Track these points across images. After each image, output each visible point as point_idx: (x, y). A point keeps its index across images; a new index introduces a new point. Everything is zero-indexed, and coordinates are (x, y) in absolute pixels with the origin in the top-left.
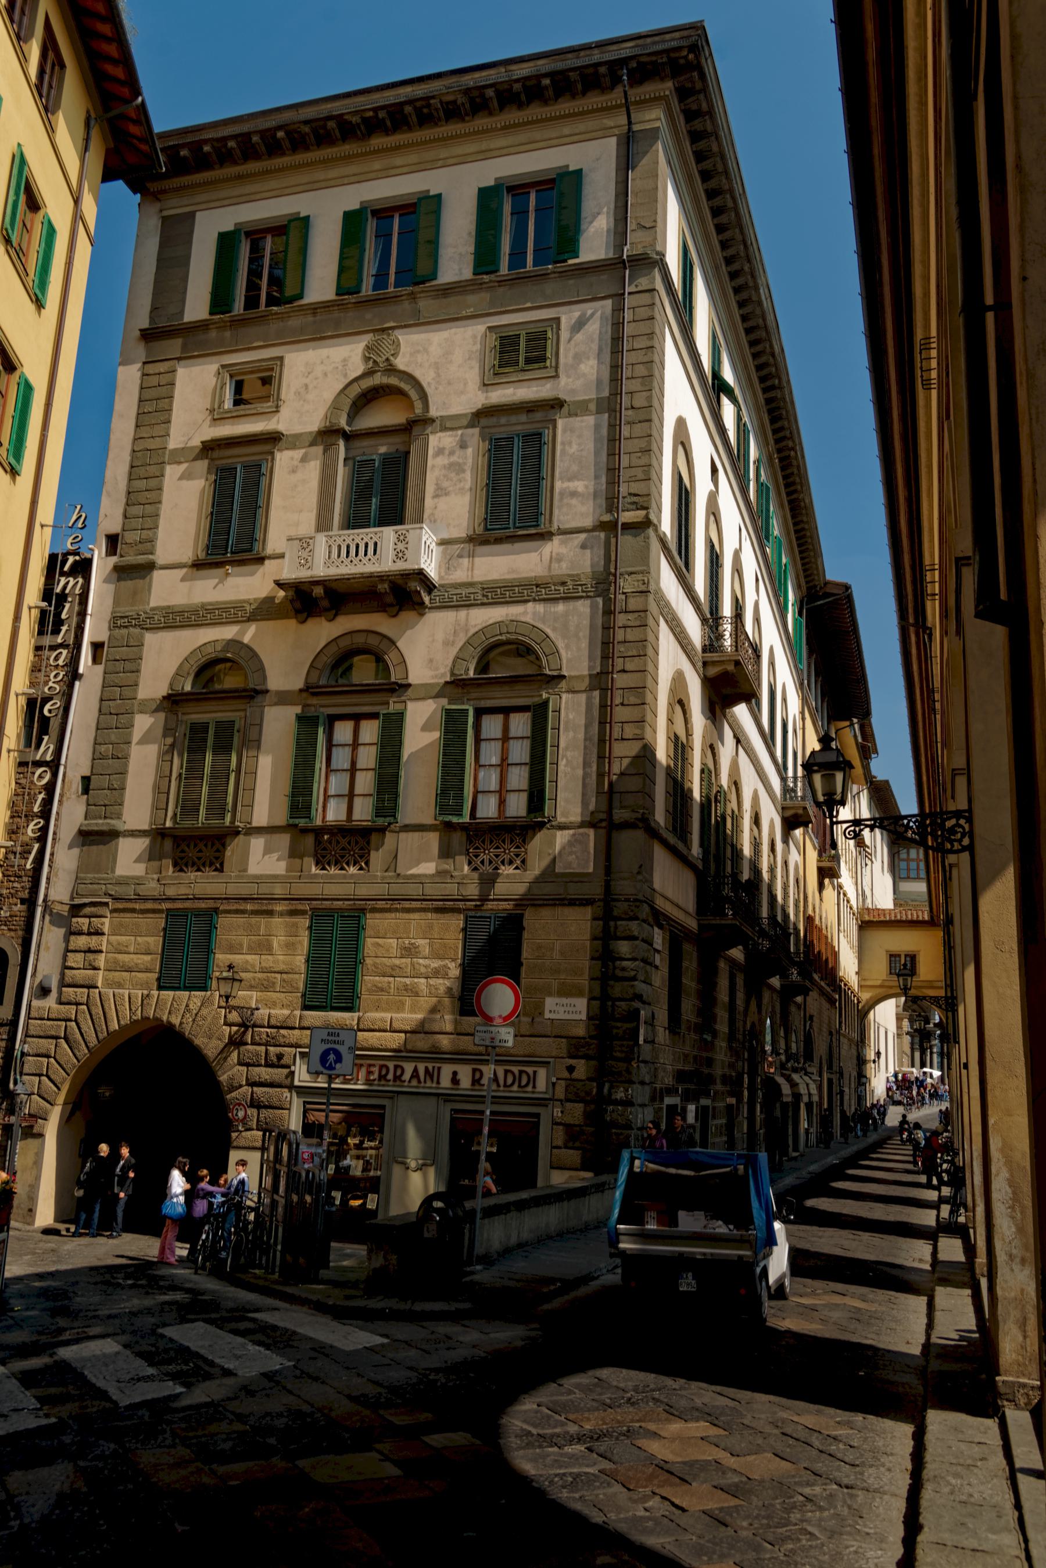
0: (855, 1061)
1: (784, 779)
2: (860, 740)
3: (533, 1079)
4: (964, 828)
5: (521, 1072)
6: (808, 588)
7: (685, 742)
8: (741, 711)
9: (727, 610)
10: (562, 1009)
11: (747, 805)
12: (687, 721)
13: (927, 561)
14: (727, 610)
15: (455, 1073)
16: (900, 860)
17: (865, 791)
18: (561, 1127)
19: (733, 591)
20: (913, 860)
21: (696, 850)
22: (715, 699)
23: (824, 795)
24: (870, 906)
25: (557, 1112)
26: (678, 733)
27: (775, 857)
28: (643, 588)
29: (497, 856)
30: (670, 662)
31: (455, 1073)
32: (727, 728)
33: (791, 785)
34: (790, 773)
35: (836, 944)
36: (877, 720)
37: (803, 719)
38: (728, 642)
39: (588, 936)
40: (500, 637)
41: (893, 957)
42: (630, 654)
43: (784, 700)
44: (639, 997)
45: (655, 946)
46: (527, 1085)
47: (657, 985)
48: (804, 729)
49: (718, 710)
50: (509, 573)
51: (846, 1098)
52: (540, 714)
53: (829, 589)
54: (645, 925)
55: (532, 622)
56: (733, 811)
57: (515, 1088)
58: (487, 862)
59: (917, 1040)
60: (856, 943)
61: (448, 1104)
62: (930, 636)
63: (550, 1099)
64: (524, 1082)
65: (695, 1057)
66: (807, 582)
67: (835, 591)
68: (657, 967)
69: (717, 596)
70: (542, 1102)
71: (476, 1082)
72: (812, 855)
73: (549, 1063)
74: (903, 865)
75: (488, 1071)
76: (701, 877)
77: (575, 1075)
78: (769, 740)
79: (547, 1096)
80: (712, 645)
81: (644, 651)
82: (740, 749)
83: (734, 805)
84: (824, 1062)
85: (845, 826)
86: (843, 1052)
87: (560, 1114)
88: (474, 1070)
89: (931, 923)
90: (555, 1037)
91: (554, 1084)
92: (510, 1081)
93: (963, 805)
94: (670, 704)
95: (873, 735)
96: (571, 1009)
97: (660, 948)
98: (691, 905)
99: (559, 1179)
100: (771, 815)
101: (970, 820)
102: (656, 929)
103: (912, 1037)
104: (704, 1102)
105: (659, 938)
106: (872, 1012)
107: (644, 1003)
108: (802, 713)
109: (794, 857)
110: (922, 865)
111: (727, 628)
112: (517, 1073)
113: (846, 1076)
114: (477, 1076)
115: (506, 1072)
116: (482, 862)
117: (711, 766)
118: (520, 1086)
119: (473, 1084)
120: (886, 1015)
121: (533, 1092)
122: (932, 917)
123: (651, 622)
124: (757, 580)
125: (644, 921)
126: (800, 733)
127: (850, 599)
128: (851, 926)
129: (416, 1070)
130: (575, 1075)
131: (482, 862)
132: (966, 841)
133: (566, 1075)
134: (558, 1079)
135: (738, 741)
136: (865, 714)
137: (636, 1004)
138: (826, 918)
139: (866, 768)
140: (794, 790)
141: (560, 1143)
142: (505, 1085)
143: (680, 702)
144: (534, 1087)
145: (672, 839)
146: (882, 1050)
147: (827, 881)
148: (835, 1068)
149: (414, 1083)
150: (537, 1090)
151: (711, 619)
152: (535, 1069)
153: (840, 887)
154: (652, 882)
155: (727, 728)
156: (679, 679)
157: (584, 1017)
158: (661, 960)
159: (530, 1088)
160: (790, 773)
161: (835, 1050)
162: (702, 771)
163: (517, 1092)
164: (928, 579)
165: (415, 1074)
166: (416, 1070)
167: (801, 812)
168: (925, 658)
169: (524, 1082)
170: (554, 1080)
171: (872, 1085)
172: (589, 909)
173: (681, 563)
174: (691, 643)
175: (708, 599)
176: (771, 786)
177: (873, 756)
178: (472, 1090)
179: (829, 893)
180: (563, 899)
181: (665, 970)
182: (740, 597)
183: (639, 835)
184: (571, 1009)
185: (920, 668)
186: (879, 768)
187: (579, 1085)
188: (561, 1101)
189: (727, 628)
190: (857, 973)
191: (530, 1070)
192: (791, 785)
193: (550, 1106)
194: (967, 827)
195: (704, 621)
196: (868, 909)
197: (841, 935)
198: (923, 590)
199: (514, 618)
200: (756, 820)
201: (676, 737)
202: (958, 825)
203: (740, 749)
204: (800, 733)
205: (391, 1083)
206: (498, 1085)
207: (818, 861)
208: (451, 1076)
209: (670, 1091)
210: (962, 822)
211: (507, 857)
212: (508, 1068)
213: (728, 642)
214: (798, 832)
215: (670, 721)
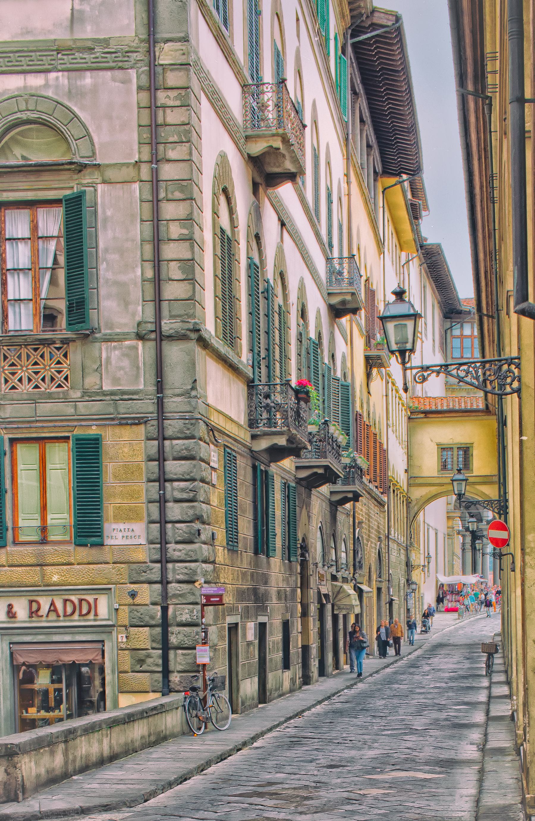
0: (403, 567)
1: (329, 260)
2: (409, 196)
3: (93, 608)
4: (514, 374)
5: (81, 601)
6: (352, 17)
7: (230, 236)
8: (286, 191)
9: (268, 75)
10: (120, 535)
11: (293, 298)
12: (231, 212)
13: (488, 49)
14: (268, 75)
15: (10, 606)
16: (453, 337)
17: (416, 262)
18: (127, 652)
19: (274, 41)
20: (467, 337)
21: (245, 358)
22: (258, 180)
23: (397, 344)
24: (420, 395)
25: (122, 638)
26: (224, 228)
27: (306, 325)
28: (182, 59)
29: (36, 373)
30: (215, 144)
31: (10, 606)
32: (336, 326)
33: (337, 267)
34: (336, 254)
35: (384, 441)
36: (429, 176)
37: (348, 183)
38: (271, 115)
39: (141, 457)
40: (19, 115)
41: (443, 449)
42: (171, 139)
43: (328, 164)
44: (199, 518)
45: (212, 464)
46: (89, 612)
47: (215, 504)
48: (349, 195)
49: (261, 190)
50: (22, 34)
51: (395, 607)
52: (75, 210)
53: (378, 19)
54: (201, 443)
55: (55, 97)
56: (280, 307)
57: (76, 616)
58: (25, 381)
59: (469, 539)
60: (405, 438)
61: (5, 638)
62: (490, 105)
63: (113, 626)
64: (84, 611)
65: (252, 575)
66: (351, 10)
67: (384, 22)
68: (214, 486)
69: (257, 55)
70: (107, 629)
71: (33, 613)
72: (359, 343)
73: (110, 589)
74: (456, 343)
75: (45, 603)
76: (250, 384)
77: (138, 600)
78: (313, 219)
79: (110, 623)
80: (256, 114)
81: (188, 134)
82: (285, 233)
83: (279, 300)
84: (373, 569)
85: (415, 371)
86: (393, 558)
87: (125, 640)
88: (31, 602)
89: (487, 411)
90: (114, 563)
91: (117, 610)
92: (69, 610)
93: (515, 354)
94: (214, 194)
95: (423, 189)
96: (129, 534)
97: (215, 465)
98: (242, 419)
99: (127, 702)
100: (316, 304)
101: (518, 366)
102: (212, 446)
103: (464, 536)
104: (262, 619)
105: (215, 456)
106: (421, 514)
107: (203, 523)
108: (347, 175)
109: (341, 347)
110: (477, 342)
111: (269, 96)
112: (77, 602)
113: (395, 582)
114: (35, 606)
115: (65, 601)
116: (20, 380)
117: (257, 261)
118: (81, 615)
119: (31, 617)
120: (436, 517)
121: (95, 620)
122: (487, 406)
123: (193, 101)
124: (298, 20)
125: (200, 439)
126: (345, 200)
127: (399, 31)
128: (400, 419)
129: (53, 604)
130: (138, 600)
131: (20, 380)
132: (515, 385)
133: (130, 600)
134: (120, 605)
135: (283, 225)
136: (415, 171)
137: (197, 525)
138: (374, 413)
139: (416, 230)
140: (340, 273)
141: (127, 667)
142: (65, 615)
143: (225, 191)
144: (96, 615)
145: (223, 349)
146: (432, 553)
147: (375, 371)
148: (385, 576)
149: (53, 616)
150: (99, 618)
151: (251, 87)
152: (96, 597)
153: (389, 375)
154: (206, 397)
155: (336, 326)
156: (223, 162)
157: (143, 541)
158: (218, 477)
159: (91, 616)
160: (336, 254)
161: (384, 555)
162: (249, 266)
163: (79, 621)
164: (489, 68)
165: (53, 608)
166: (53, 604)
167: (348, 298)
168: (485, 128)
169: (84, 611)
170: (116, 606)
171: (422, 591)
172: (142, 429)
173: (219, 19)
174: (232, 119)
175: (248, 58)
176: (316, 271)
177: (424, 213)
178: (9, 622)
179: (377, 385)
180: (113, 419)
181: (221, 488)
182: (280, 49)
183: (193, 346)
184: (129, 534)
185: (478, 139)
186: (431, 230)
187: (142, 609)
188: (125, 626)
189: (269, 96)
190: (406, 471)
191: (90, 598)
192: (337, 267)
193: (114, 634)
194: (516, 371)
195: (244, 86)
196: (418, 398)
197: (390, 430)
198: (483, 66)
199: (33, 92)
200: (303, 314)
201: (223, 231)
202: (509, 371)
203: (285, 233)
204: (345, 200)
205: (44, 618)
206: (58, 616)
207: (365, 350)
208: (6, 609)
209: (232, 611)
210: (513, 367)
211: (48, 375)
212: (66, 597)
213: (271, 115)
214: (345, 320)
215: (215, 213)
